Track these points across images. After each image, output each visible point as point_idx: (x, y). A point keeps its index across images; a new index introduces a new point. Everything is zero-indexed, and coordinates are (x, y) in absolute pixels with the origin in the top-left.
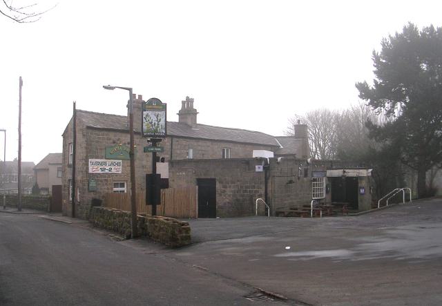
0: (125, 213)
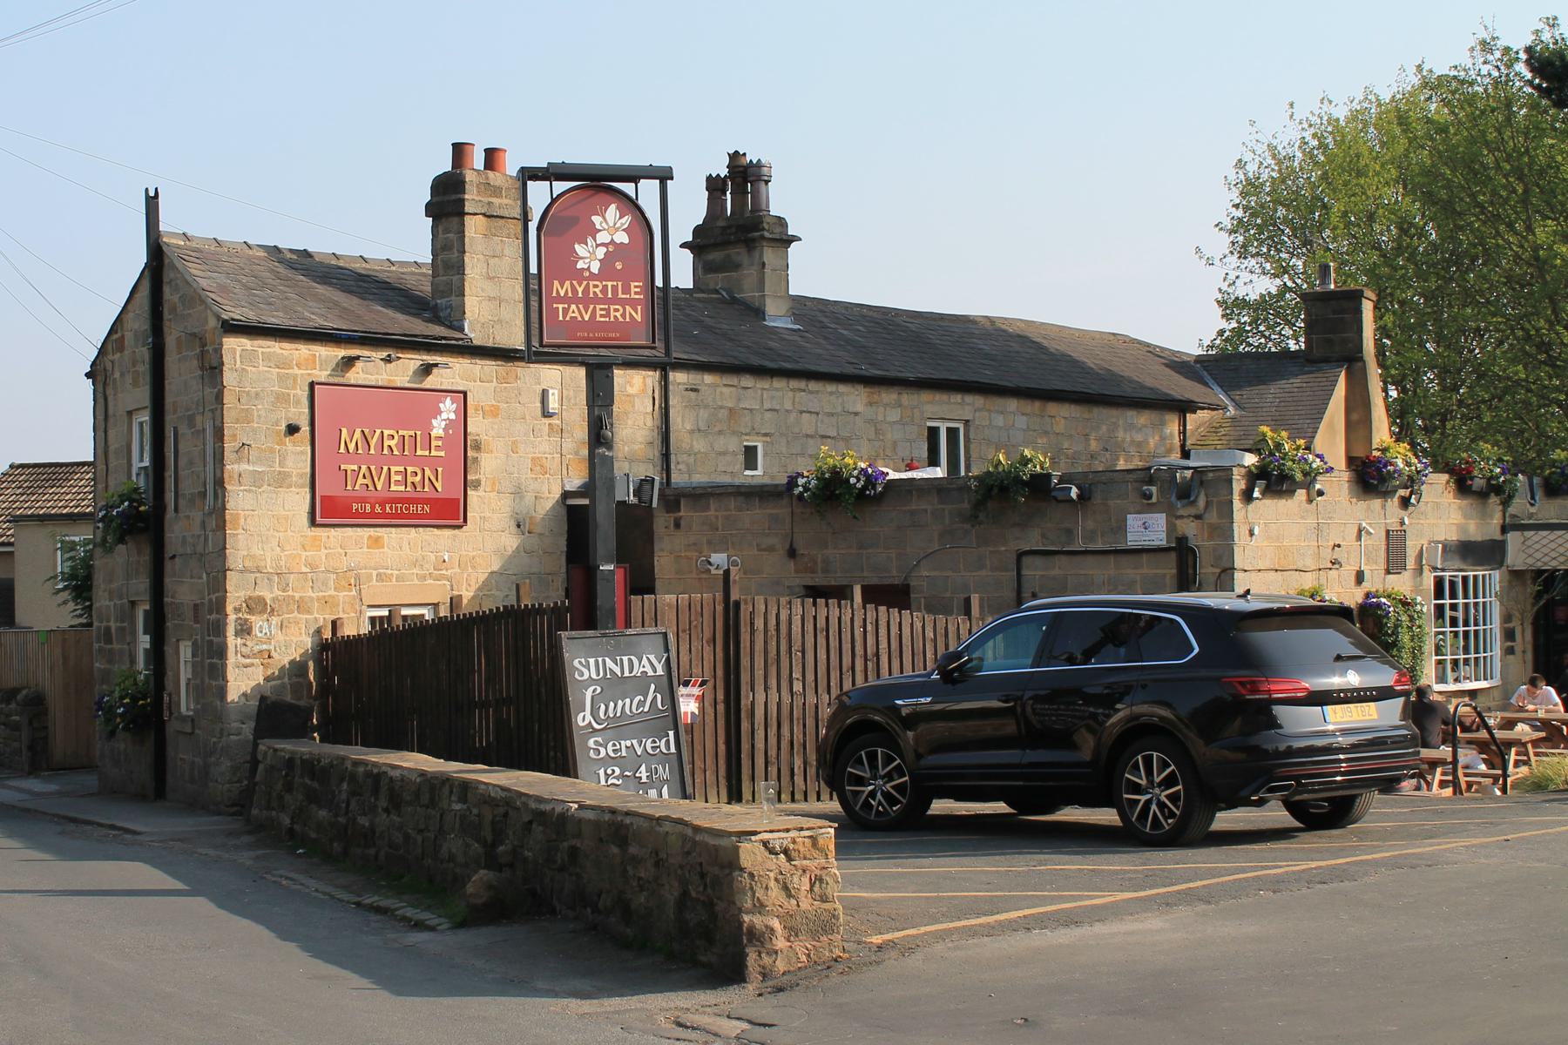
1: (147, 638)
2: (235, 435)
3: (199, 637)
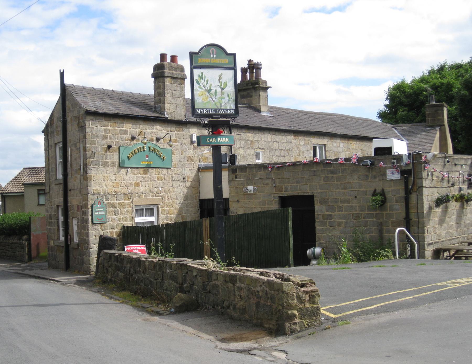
0: (167, 262)
1: (63, 218)
2: (90, 149)
3: (79, 217)
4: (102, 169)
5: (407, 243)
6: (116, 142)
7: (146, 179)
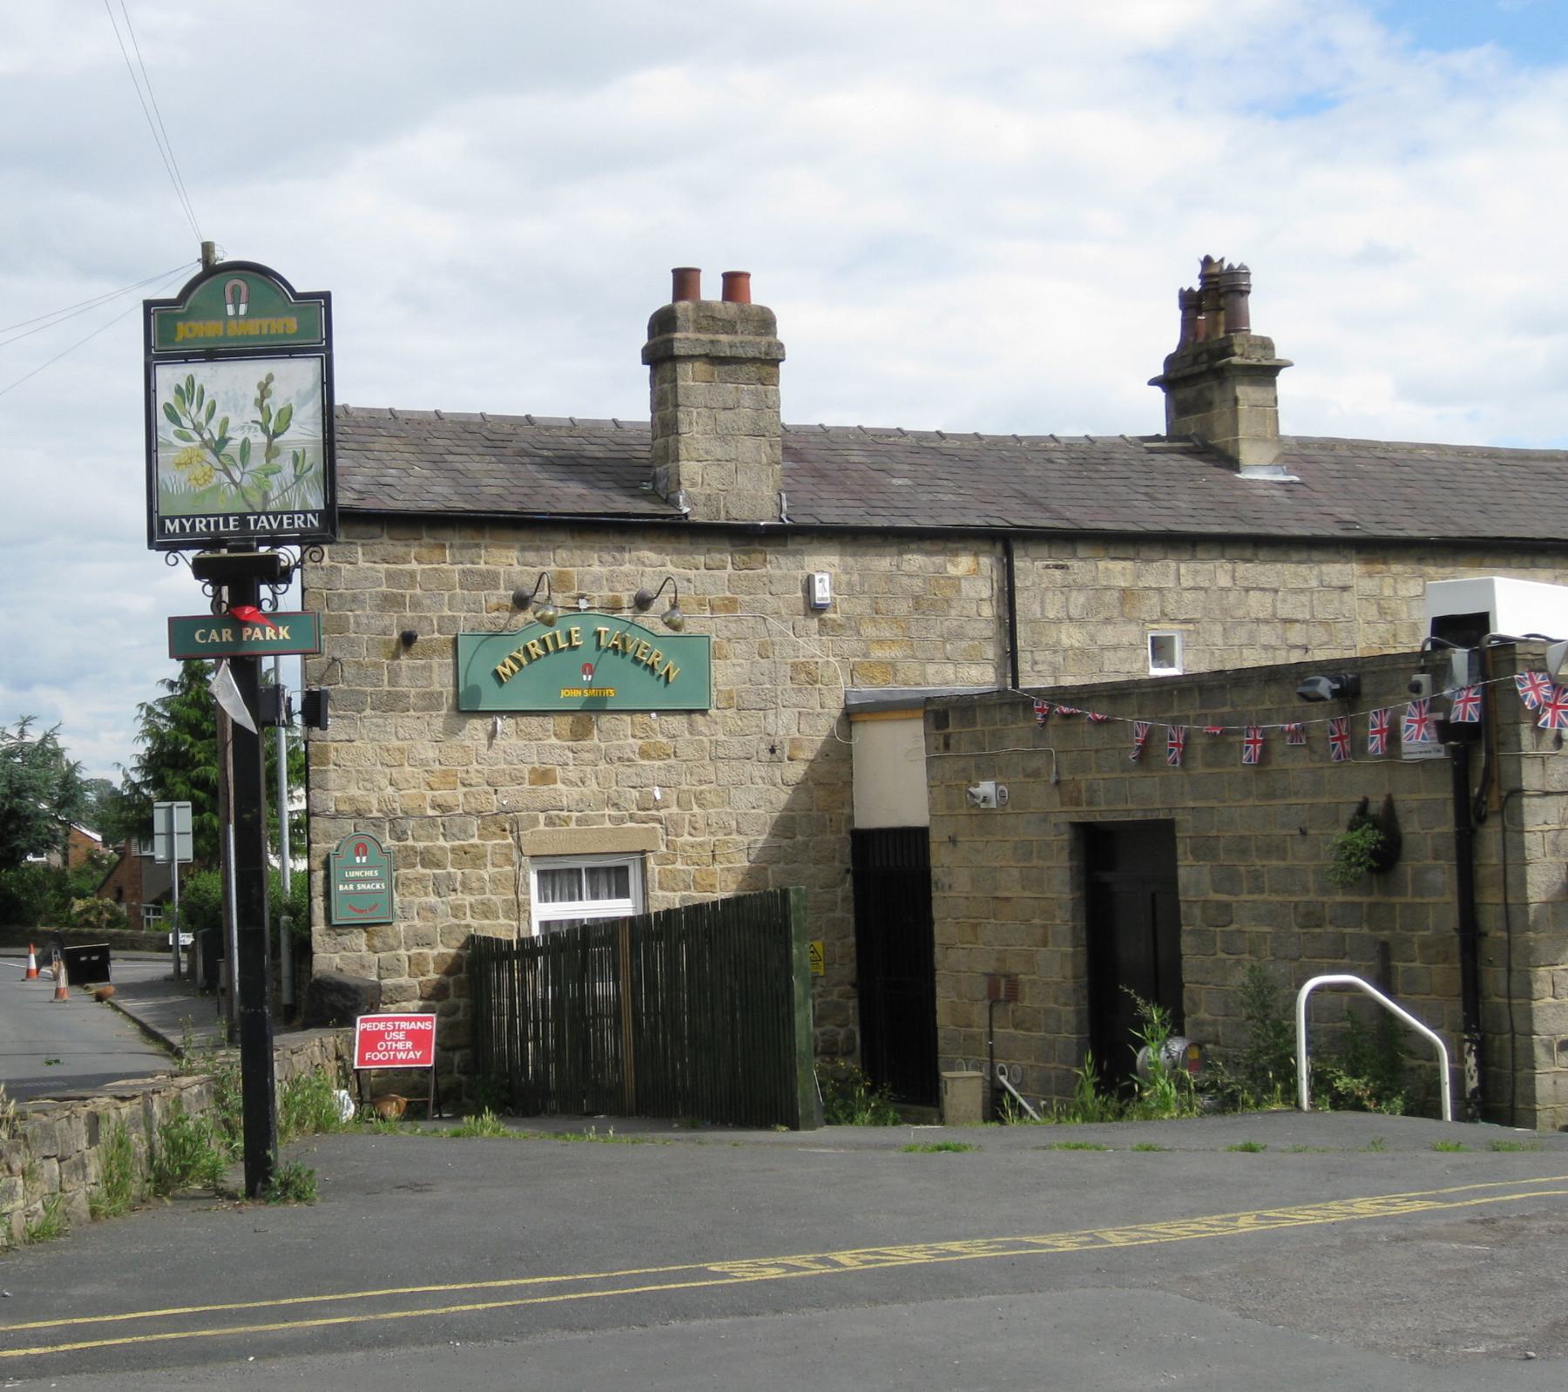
4: (374, 720)
5: (1466, 1037)
6: (441, 618)
7: (586, 756)
